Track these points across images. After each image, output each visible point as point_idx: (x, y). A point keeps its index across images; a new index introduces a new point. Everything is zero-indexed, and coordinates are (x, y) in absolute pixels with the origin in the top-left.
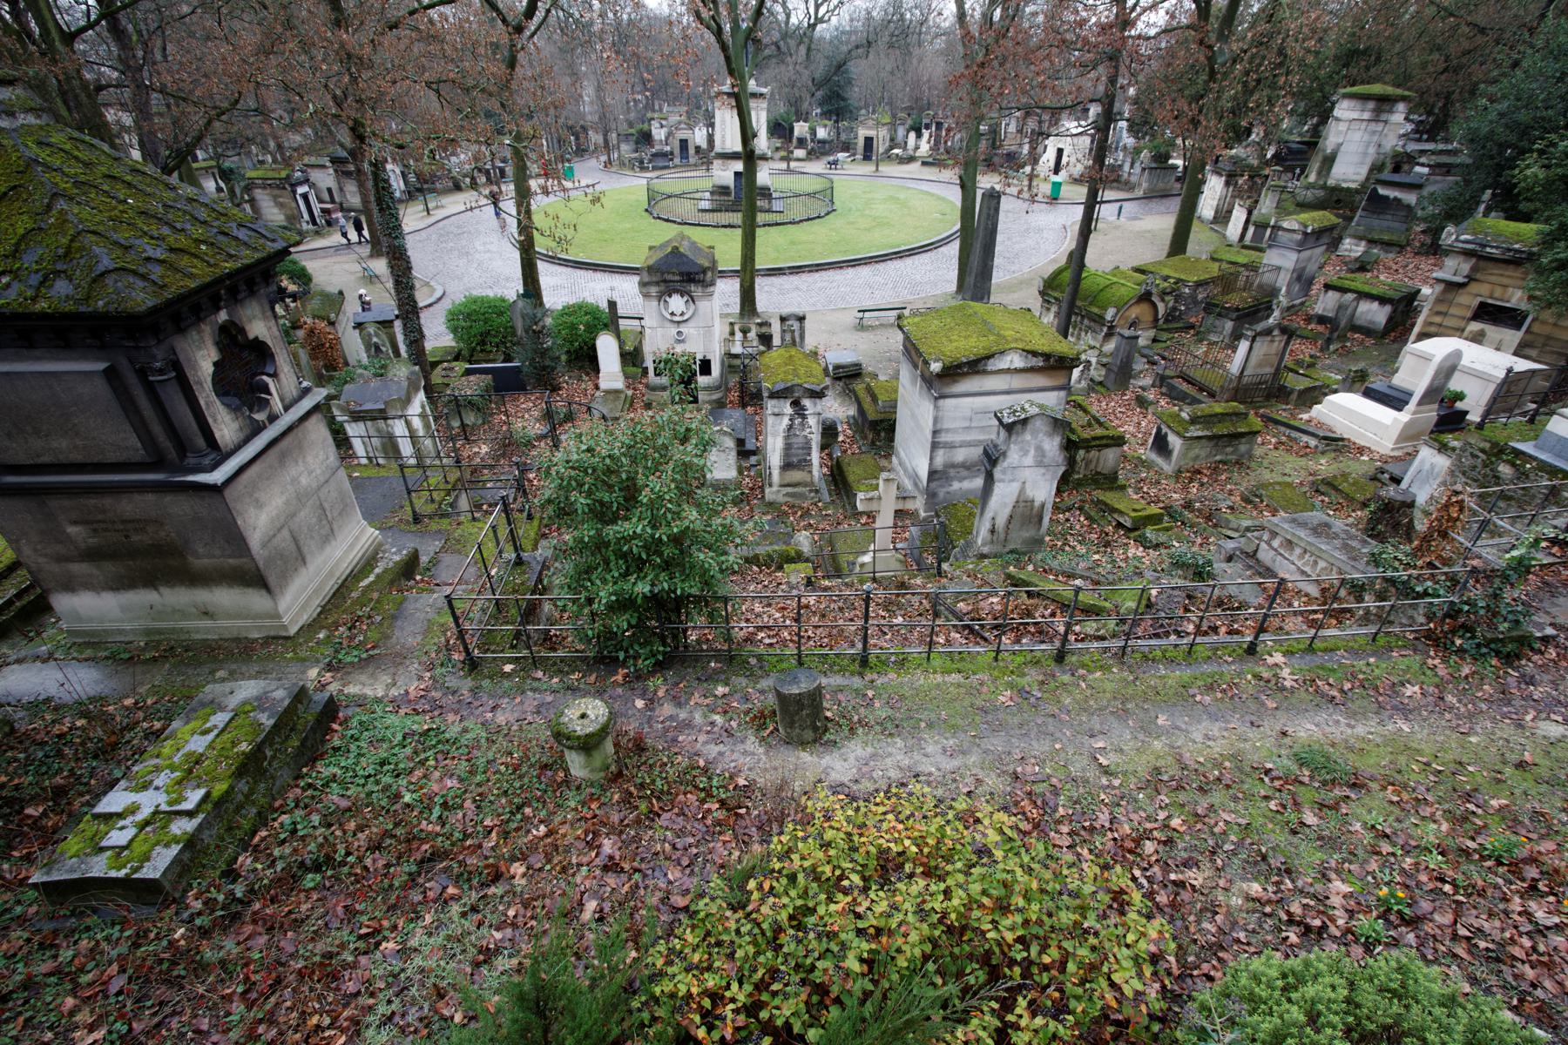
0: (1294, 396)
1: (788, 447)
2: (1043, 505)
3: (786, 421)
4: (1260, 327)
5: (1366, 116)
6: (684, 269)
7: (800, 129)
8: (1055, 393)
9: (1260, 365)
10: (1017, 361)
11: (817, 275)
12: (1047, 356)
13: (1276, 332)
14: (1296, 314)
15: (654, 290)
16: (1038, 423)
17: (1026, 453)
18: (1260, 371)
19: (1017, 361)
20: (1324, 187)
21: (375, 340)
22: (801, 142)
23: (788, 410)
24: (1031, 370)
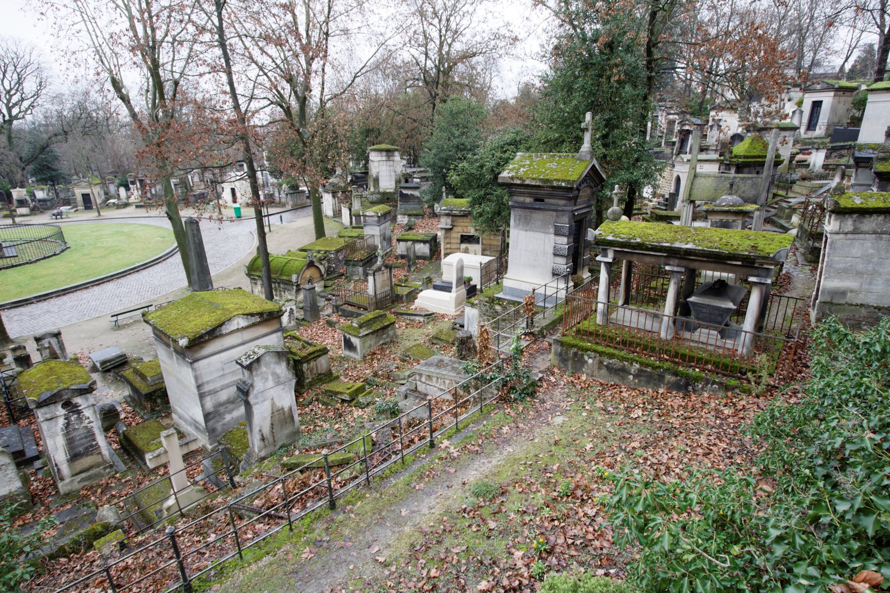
2: (290, 409)
9: (382, 287)
10: (242, 322)
12: (261, 314)
16: (267, 358)
17: (266, 380)
19: (242, 322)
23: (60, 411)
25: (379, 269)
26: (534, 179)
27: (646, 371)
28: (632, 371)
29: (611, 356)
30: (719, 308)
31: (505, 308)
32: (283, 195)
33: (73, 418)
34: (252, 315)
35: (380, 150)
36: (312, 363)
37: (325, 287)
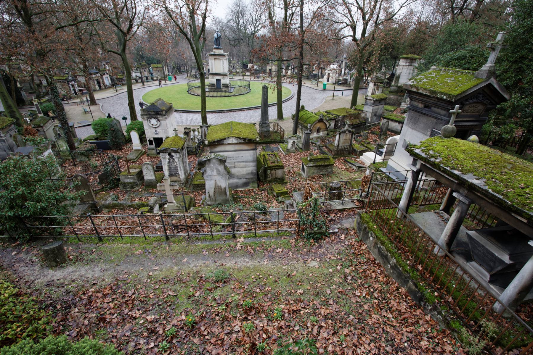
0: (358, 153)
1: (170, 169)
2: (225, 188)
3: (167, 160)
4: (341, 131)
5: (408, 64)
6: (155, 110)
7: (250, 66)
8: (252, 151)
9: (344, 143)
10: (235, 141)
11: (235, 113)
12: (244, 139)
13: (347, 132)
14: (377, 126)
15: (145, 117)
16: (214, 161)
17: (213, 171)
18: (344, 145)
19: (235, 141)
20: (397, 86)
21: (58, 132)
22: (249, 70)
23: (168, 157)
24: (240, 143)
25: (344, 132)
26: (425, 89)
27: (398, 269)
28: (391, 262)
29: (383, 243)
30: (493, 255)
31: (382, 179)
32: (351, 81)
33: (171, 160)
34: (240, 138)
35: (406, 58)
36: (273, 171)
37: (328, 134)
